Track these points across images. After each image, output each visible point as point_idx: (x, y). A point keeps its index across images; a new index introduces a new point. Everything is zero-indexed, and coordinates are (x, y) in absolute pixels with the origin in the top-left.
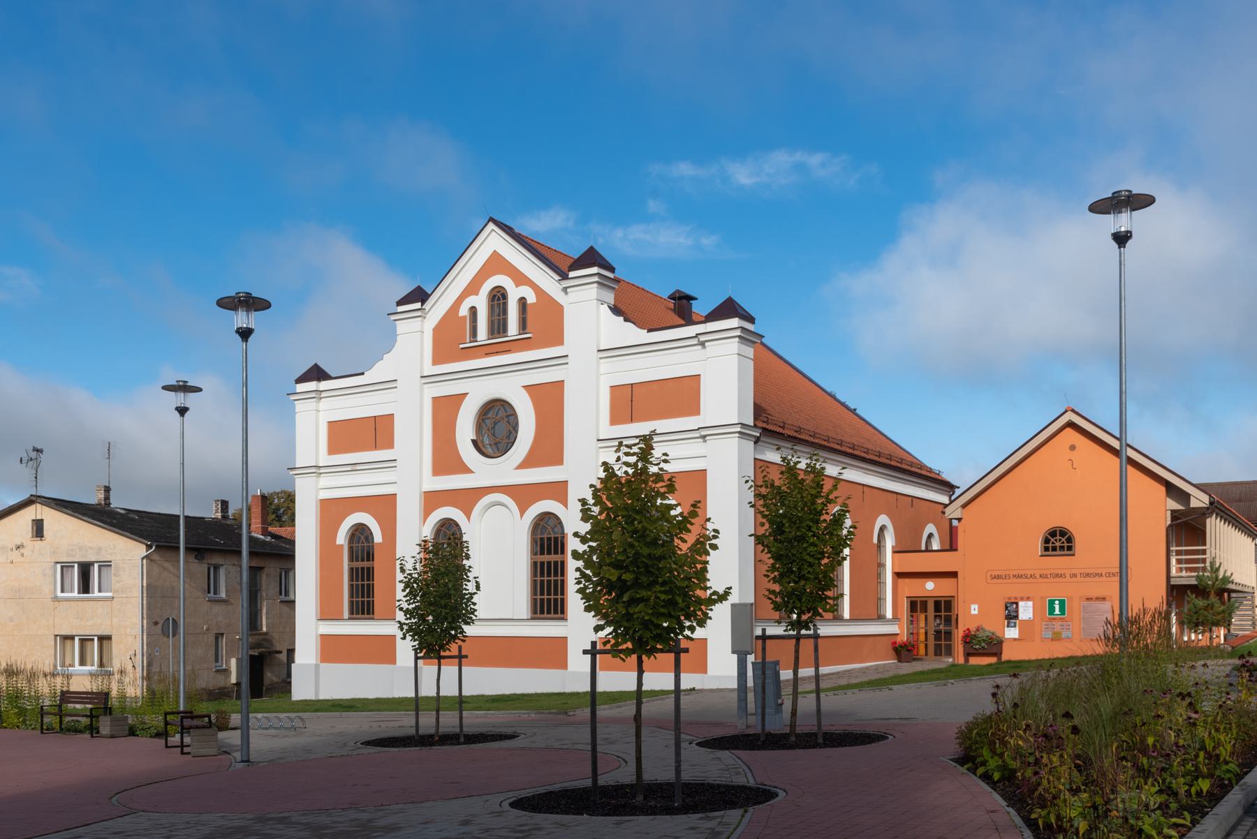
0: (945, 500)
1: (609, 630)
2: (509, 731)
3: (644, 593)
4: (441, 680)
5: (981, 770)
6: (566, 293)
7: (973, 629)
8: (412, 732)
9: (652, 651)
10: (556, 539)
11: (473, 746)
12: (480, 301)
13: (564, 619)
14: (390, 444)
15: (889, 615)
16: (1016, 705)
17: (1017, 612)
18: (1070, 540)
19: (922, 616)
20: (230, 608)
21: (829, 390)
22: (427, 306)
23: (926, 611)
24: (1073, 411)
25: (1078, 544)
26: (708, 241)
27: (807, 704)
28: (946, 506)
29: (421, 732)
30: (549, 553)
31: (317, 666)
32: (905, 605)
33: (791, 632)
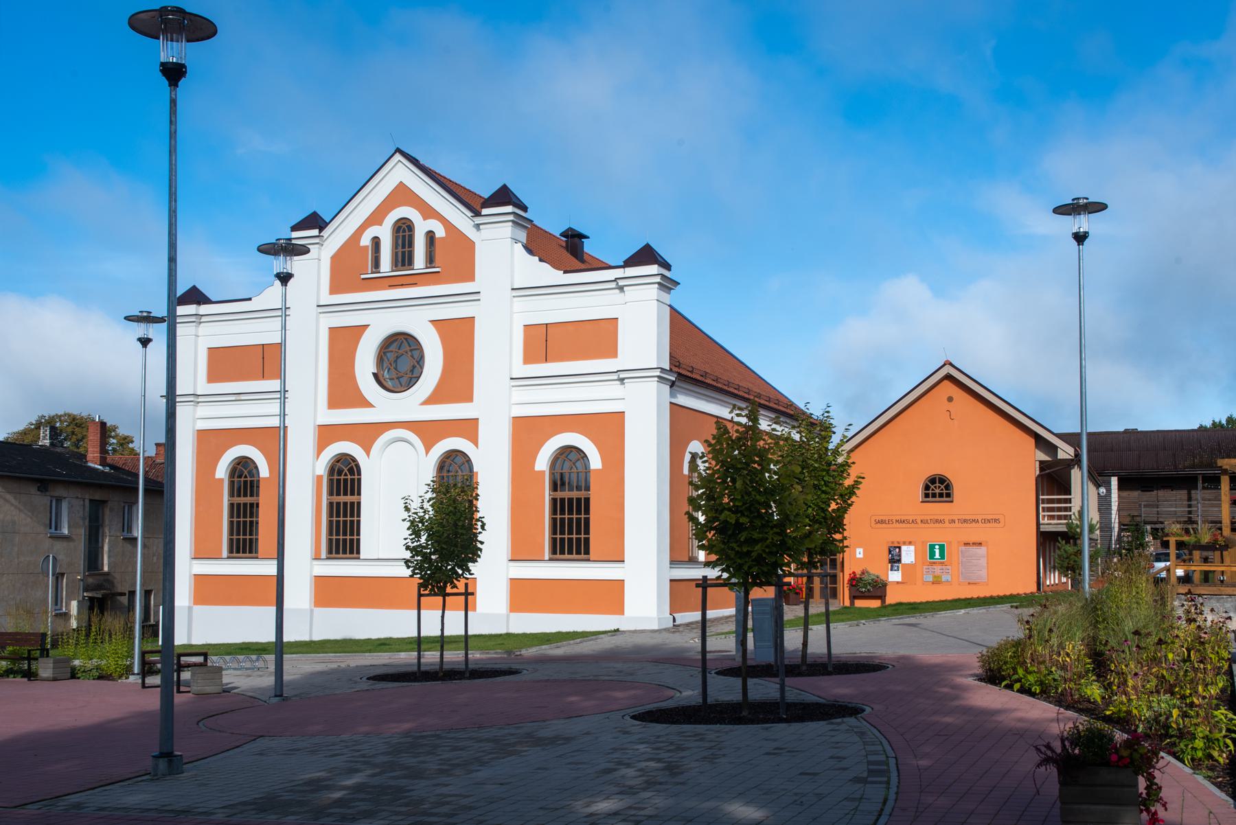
3: (756, 535)
5: (1017, 686)
8: (415, 669)
12: (384, 231)
18: (948, 487)
20: (71, 544)
22: (325, 233)
25: (957, 491)
29: (423, 669)
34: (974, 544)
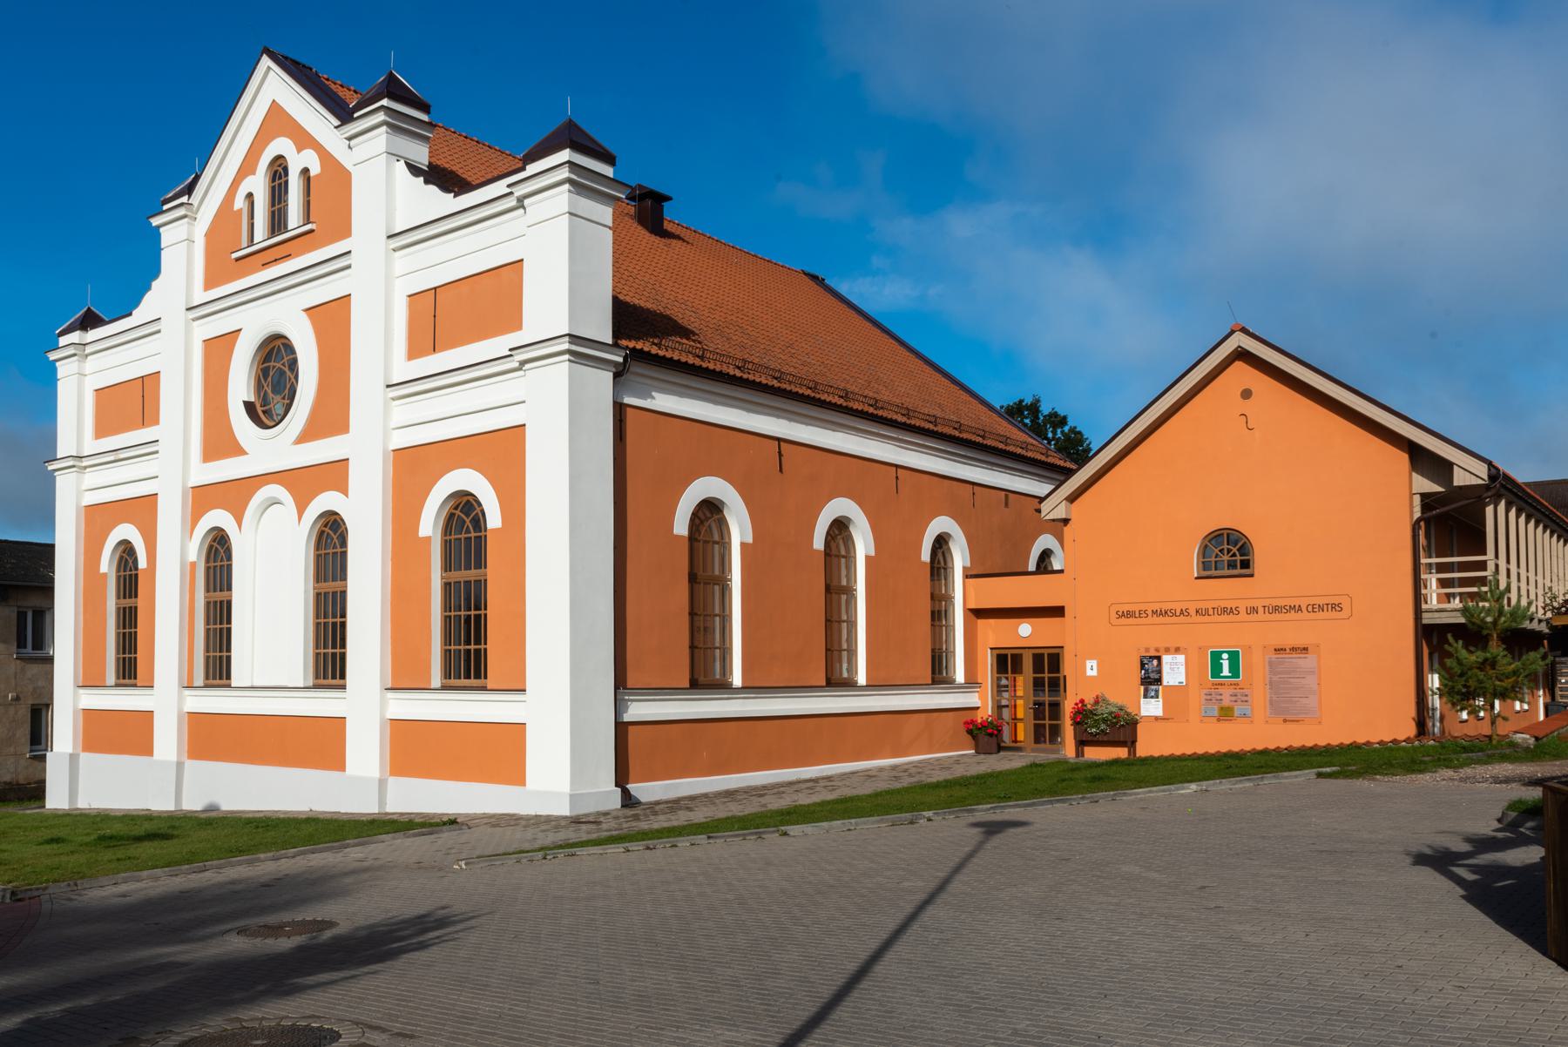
7: (1089, 700)
12: (258, 184)
14: (156, 422)
15: (960, 677)
17: (1160, 672)
24: (1244, 330)
28: (1042, 500)
32: (987, 662)
34: (1293, 649)
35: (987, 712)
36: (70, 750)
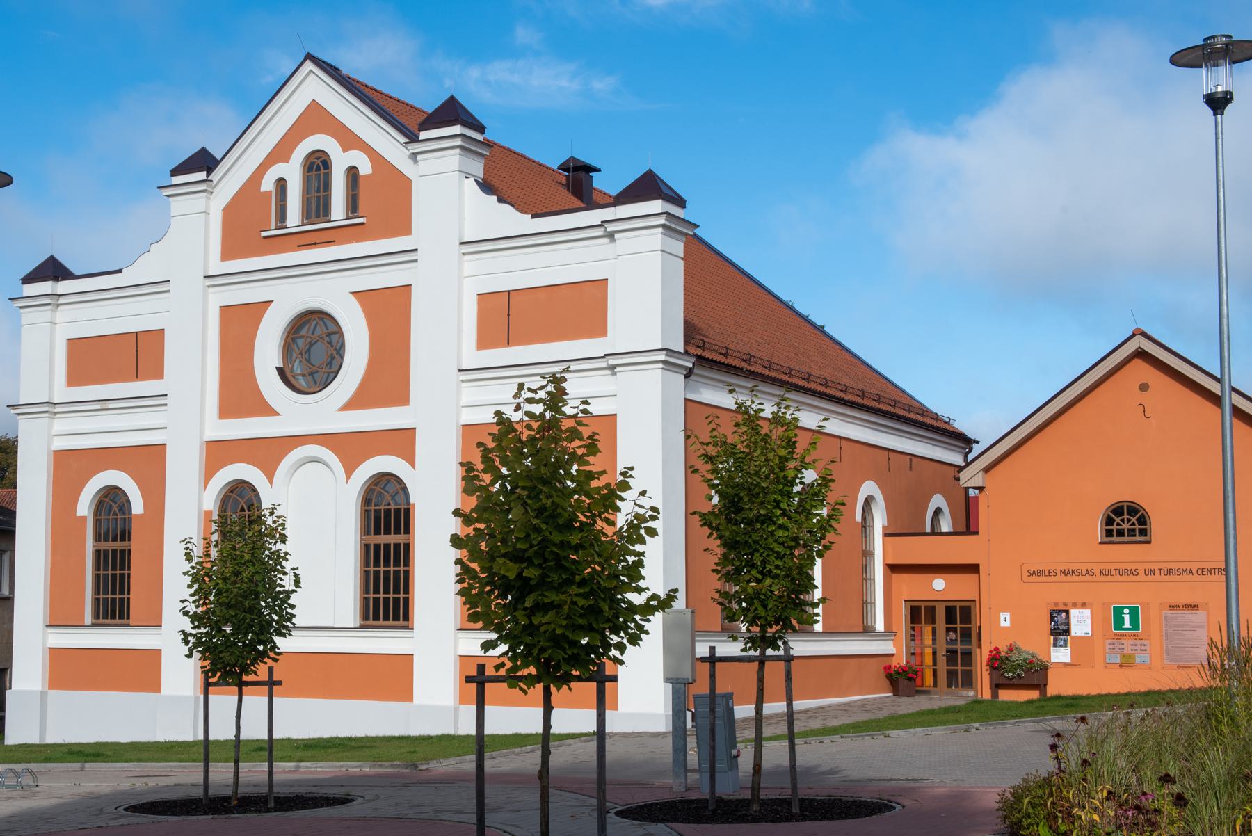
0: (957, 459)
1: (503, 648)
2: (339, 792)
3: (553, 597)
4: (241, 716)
6: (416, 161)
7: (1003, 649)
8: (199, 793)
9: (566, 679)
10: (398, 511)
11: (289, 814)
12: (292, 170)
13: (409, 628)
14: (158, 373)
15: (880, 626)
16: (1085, 763)
17: (1068, 624)
18: (1143, 520)
19: (928, 629)
21: (785, 298)
22: (215, 176)
23: (934, 622)
25: (1155, 527)
26: (602, 85)
27: (776, 754)
28: (961, 469)
29: (211, 793)
30: (387, 532)
31: (43, 695)
32: (903, 613)
33: (752, 653)
34: (1185, 606)
35: (902, 660)
36: (39, 688)
